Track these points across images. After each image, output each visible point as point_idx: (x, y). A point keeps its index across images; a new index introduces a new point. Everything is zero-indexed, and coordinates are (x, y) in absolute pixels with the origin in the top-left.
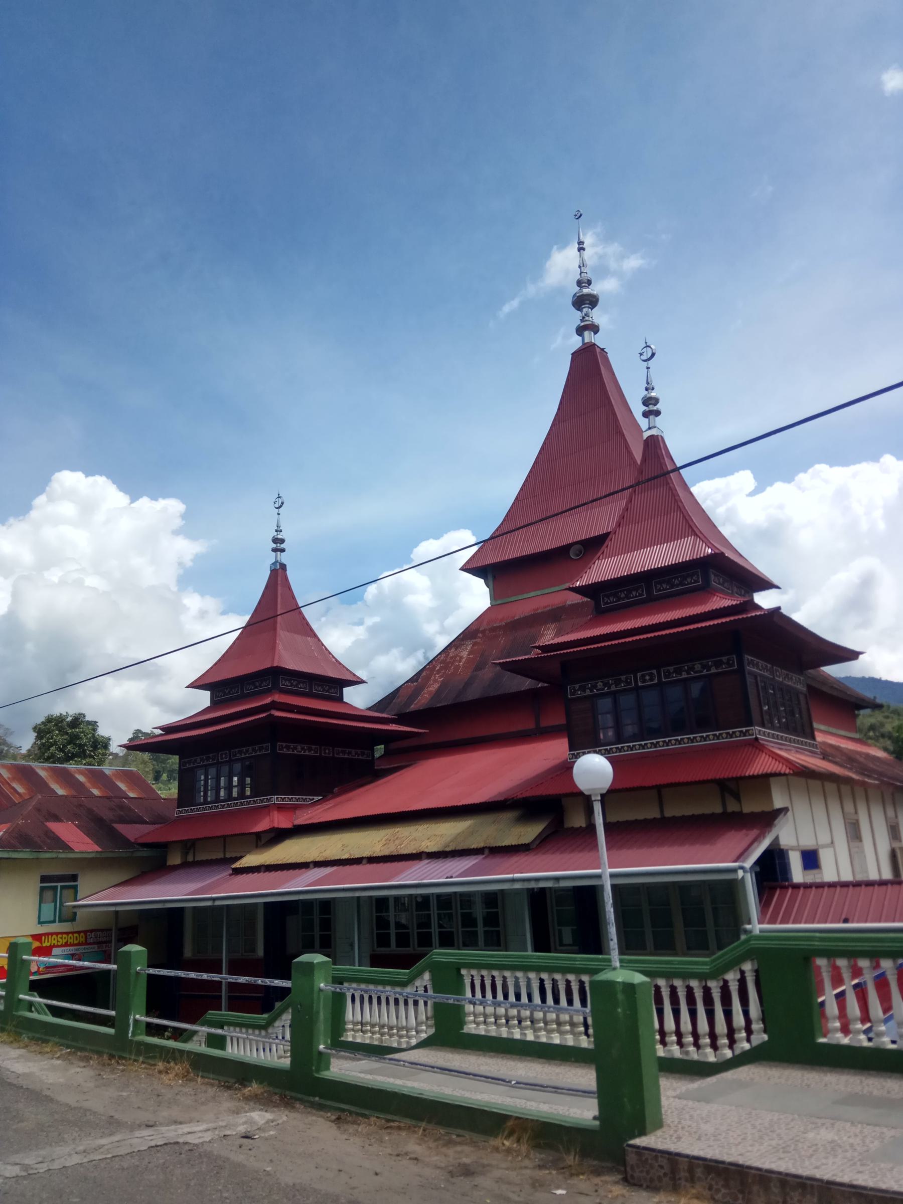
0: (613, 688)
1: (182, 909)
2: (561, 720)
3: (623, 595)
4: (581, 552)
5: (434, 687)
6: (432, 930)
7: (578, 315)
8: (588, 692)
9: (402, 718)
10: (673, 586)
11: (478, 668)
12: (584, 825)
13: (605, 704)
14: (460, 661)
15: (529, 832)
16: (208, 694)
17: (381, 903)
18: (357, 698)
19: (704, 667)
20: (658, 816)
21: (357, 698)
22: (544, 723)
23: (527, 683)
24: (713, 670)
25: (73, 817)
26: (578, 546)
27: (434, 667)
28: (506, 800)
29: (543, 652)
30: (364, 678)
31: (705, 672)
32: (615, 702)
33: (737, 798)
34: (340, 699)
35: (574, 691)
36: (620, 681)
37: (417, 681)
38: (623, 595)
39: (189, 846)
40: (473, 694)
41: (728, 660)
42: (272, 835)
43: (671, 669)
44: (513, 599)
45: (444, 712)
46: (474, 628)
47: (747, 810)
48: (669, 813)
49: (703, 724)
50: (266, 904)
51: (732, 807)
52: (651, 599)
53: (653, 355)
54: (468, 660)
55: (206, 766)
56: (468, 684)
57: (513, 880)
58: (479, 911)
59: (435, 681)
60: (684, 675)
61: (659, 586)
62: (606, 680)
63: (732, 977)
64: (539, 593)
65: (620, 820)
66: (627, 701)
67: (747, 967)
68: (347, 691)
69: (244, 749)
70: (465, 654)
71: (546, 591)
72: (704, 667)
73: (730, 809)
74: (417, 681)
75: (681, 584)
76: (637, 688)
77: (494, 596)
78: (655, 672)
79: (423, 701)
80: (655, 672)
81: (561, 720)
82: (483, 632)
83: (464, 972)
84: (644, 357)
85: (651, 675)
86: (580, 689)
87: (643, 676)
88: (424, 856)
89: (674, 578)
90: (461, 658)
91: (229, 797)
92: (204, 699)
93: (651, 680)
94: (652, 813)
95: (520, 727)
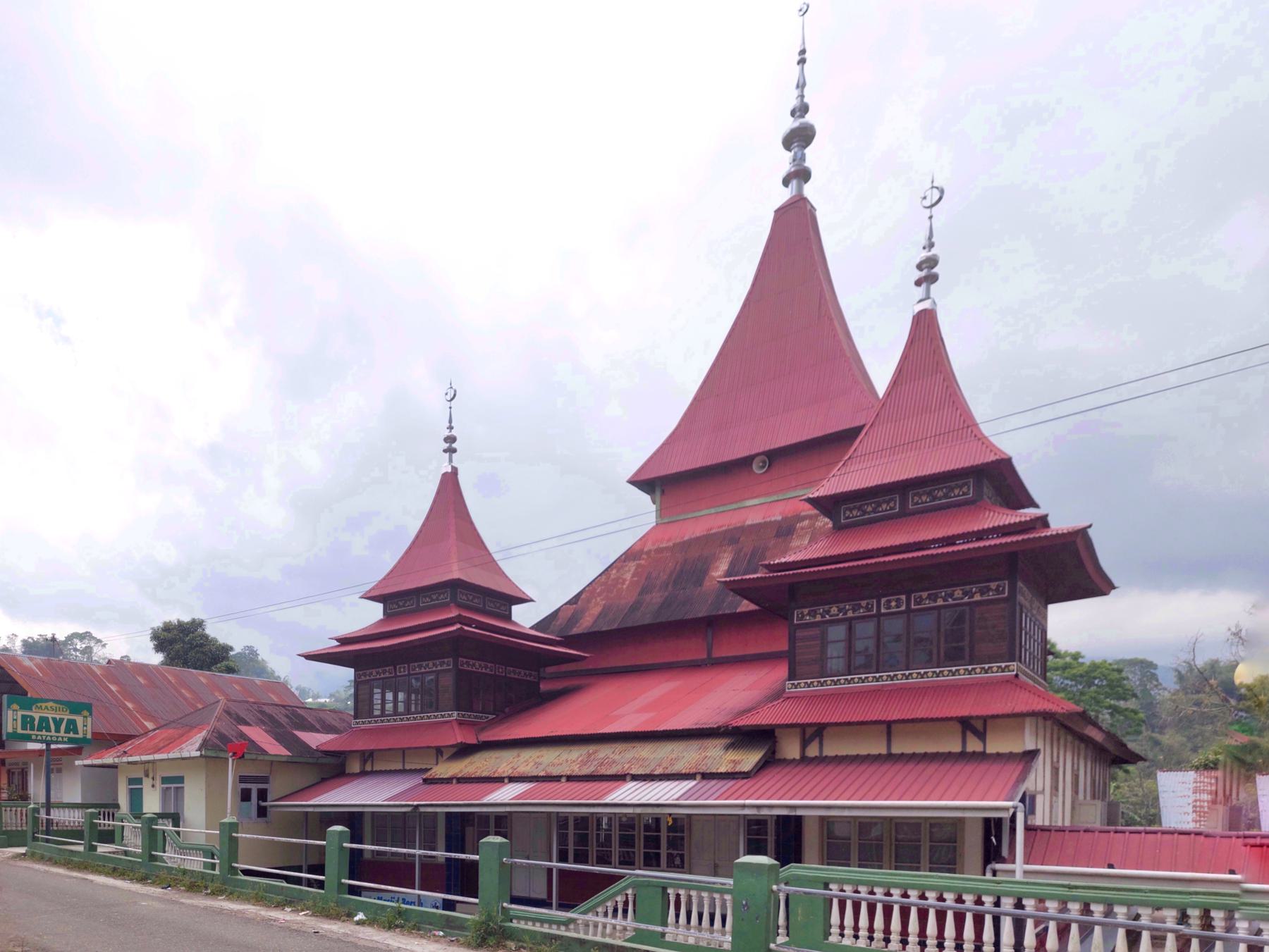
0: (850, 614)
1: (361, 814)
2: (783, 646)
3: (869, 509)
4: (764, 462)
5: (595, 610)
6: (636, 850)
7: (788, 156)
8: (819, 618)
9: (568, 641)
10: (935, 498)
11: (645, 590)
12: (798, 757)
13: (837, 632)
14: (623, 583)
15: (749, 759)
16: (380, 606)
17: (582, 822)
18: (525, 617)
19: (965, 594)
20: (884, 751)
21: (525, 617)
22: (719, 653)
23: (746, 606)
24: (977, 598)
25: (261, 722)
26: (763, 457)
27: (595, 589)
28: (719, 728)
29: (771, 571)
30: (532, 596)
31: (966, 599)
32: (850, 629)
33: (982, 736)
34: (508, 618)
35: (802, 615)
36: (860, 606)
37: (576, 603)
38: (869, 509)
39: (367, 756)
40: (644, 617)
41: (998, 586)
42: (454, 750)
43: (925, 594)
44: (682, 517)
45: (627, 633)
46: (637, 548)
47: (992, 748)
48: (896, 750)
49: (954, 656)
50: (448, 814)
51: (974, 745)
52: (904, 514)
53: (942, 192)
54: (631, 582)
55: (851, 619)
56: (635, 607)
57: (744, 806)
58: (640, 836)
59: (597, 604)
60: (940, 602)
61: (916, 499)
62: (842, 605)
63: (620, 899)
64: (713, 511)
65: (840, 754)
66: (866, 630)
67: (630, 892)
68: (515, 608)
69: (424, 664)
70: (628, 576)
71: (721, 509)
72: (965, 594)
73: (970, 749)
74: (576, 603)
75: (946, 496)
76: (879, 615)
77: (661, 512)
78: (903, 597)
79: (585, 624)
80: (903, 597)
81: (783, 646)
82: (648, 553)
83: (670, 891)
84: (927, 203)
85: (898, 600)
86: (809, 614)
87: (889, 601)
88: (628, 778)
89: (938, 490)
90: (624, 581)
91: (396, 712)
92: (375, 612)
93: (897, 606)
94: (879, 748)
95: (689, 657)
